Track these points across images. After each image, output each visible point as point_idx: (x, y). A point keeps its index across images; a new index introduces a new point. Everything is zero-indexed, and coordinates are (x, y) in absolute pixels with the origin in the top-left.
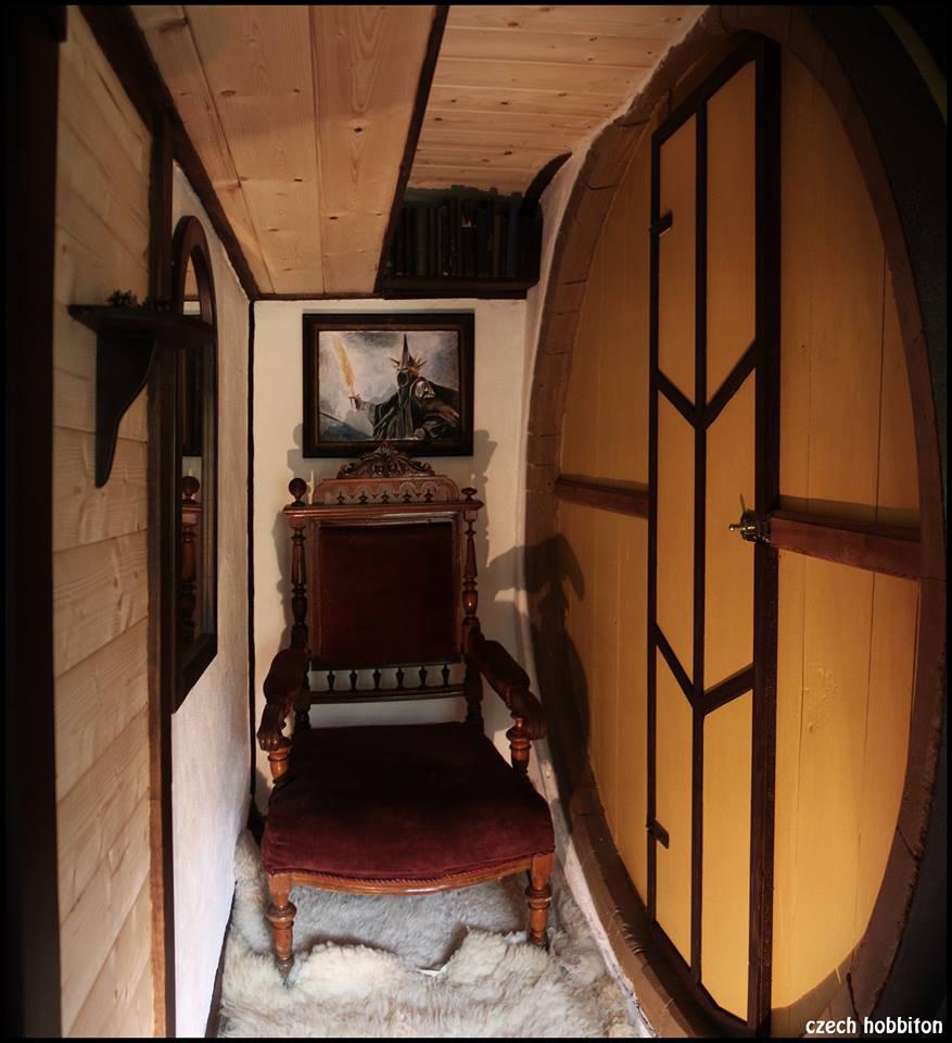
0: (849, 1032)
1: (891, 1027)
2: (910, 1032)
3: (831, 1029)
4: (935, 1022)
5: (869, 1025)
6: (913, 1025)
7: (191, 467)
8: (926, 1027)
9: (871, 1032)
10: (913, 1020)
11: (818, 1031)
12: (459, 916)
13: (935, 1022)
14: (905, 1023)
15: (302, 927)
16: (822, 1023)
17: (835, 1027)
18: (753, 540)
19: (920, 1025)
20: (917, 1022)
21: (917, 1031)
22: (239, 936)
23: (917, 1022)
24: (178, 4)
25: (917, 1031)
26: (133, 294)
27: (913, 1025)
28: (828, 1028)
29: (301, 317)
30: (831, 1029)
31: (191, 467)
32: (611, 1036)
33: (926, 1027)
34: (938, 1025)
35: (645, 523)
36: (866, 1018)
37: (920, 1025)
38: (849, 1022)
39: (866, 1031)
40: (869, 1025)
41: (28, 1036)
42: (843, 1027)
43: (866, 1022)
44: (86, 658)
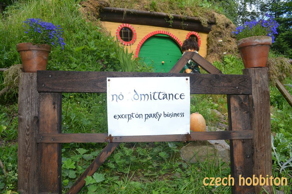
1: (263, 181)
2: (267, 184)
3: (218, 183)
5: (242, 180)
6: (269, 180)
7: (286, 97)
8: (277, 181)
10: (269, 177)
12: (33, 85)
14: (257, 178)
16: (213, 179)
17: (221, 182)
18: (185, 75)
22: (207, 143)
23: (271, 178)
24: (124, 23)
25: (272, 184)
27: (269, 180)
28: (216, 182)
30: (218, 183)
31: (286, 97)
33: (277, 181)
34: (231, 180)
36: (240, 176)
38: (230, 178)
39: (240, 184)
40: (242, 180)
43: (240, 178)
44: (144, 42)
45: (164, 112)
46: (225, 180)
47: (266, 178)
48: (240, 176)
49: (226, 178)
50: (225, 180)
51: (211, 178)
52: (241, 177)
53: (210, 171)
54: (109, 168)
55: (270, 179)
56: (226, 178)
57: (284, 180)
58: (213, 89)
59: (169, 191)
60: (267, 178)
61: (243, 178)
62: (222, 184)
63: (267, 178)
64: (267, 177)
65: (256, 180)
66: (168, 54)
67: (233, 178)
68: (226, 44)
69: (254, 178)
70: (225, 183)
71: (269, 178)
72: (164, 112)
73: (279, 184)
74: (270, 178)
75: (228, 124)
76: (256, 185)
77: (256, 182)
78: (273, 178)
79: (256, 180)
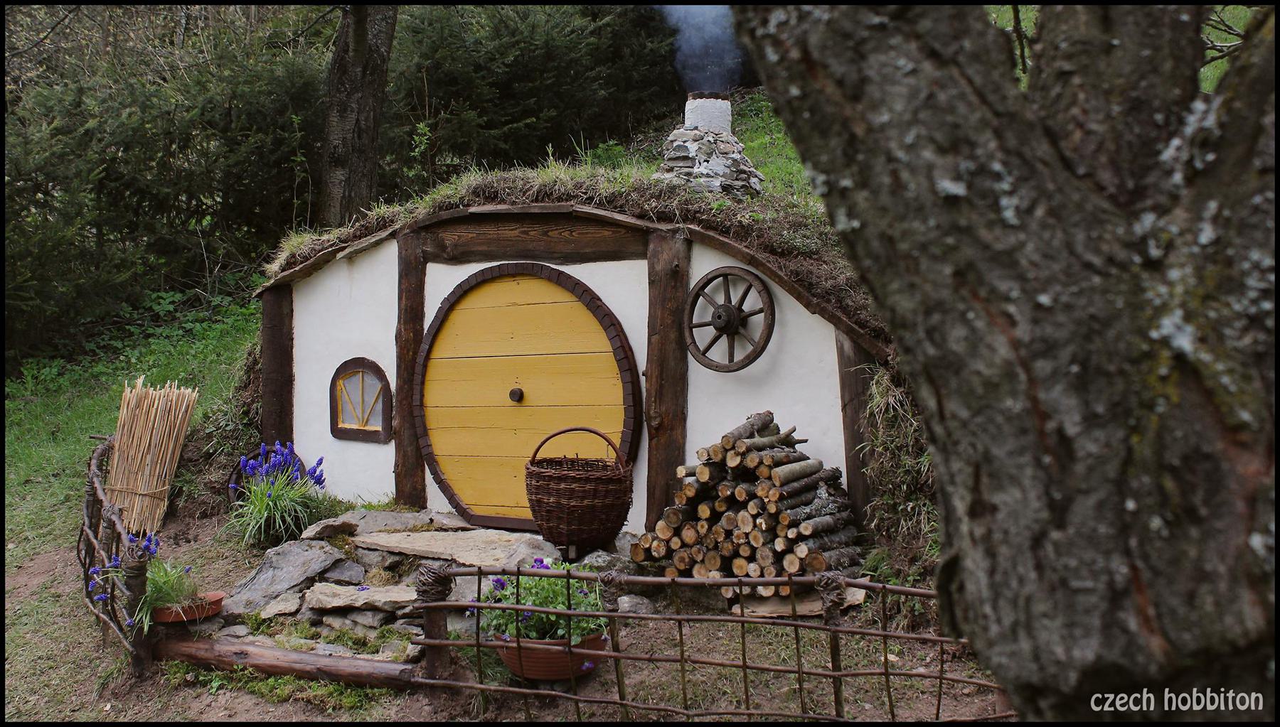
0: (1145, 708)
3: (1122, 705)
4: (1254, 695)
5: (1170, 699)
6: (1226, 699)
10: (1226, 692)
11: (1106, 708)
16: (1112, 696)
17: (1128, 702)
19: (1234, 699)
20: (1231, 694)
21: (1231, 707)
25: (1231, 707)
27: (1226, 699)
28: (1118, 703)
30: (1122, 705)
34: (1149, 699)
36: (1167, 690)
37: (1234, 699)
38: (1145, 696)
39: (1166, 708)
40: (1170, 699)
42: (1138, 702)
43: (1167, 696)
45: (806, 441)
48: (1167, 690)
58: (1060, 190)
61: (1173, 695)
65: (1212, 698)
66: (518, 396)
67: (1151, 695)
68: (740, 201)
69: (1195, 695)
70: (1136, 705)
72: (806, 441)
77: (1212, 703)
79: (1212, 698)
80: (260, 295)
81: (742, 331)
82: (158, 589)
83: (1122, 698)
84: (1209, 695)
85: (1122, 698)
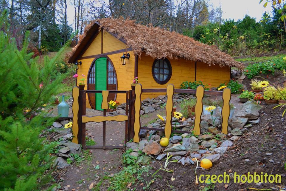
1: (257, 178)
3: (215, 180)
4: (277, 176)
6: (264, 178)
8: (271, 179)
9: (239, 182)
10: (264, 174)
13: (277, 176)
14: (258, 175)
15: (122, 59)
16: (209, 176)
19: (267, 177)
20: (266, 175)
26: (6, 133)
27: (264, 178)
29: (131, 87)
30: (215, 180)
32: (96, 90)
34: (227, 178)
35: (119, 94)
37: (267, 177)
38: (225, 176)
39: (235, 182)
41: (140, 67)
42: (221, 178)
45: (260, 3)
46: (220, 177)
47: (260, 175)
49: (222, 176)
50: (220, 177)
51: (206, 176)
52: (226, 174)
53: (278, 91)
54: (151, 174)
55: (264, 177)
56: (222, 176)
57: (251, 177)
59: (266, 74)
60: (262, 176)
62: (217, 181)
63: (262, 176)
64: (205, 176)
65: (257, 177)
71: (263, 176)
72: (260, 3)
73: (252, 181)
74: (264, 175)
75: (102, 54)
76: (250, 182)
78: (267, 175)
79: (257, 177)
80: (100, 31)
81: (15, 185)
82: (185, 57)
83: (214, 177)
84: (255, 175)
85: (214, 177)
